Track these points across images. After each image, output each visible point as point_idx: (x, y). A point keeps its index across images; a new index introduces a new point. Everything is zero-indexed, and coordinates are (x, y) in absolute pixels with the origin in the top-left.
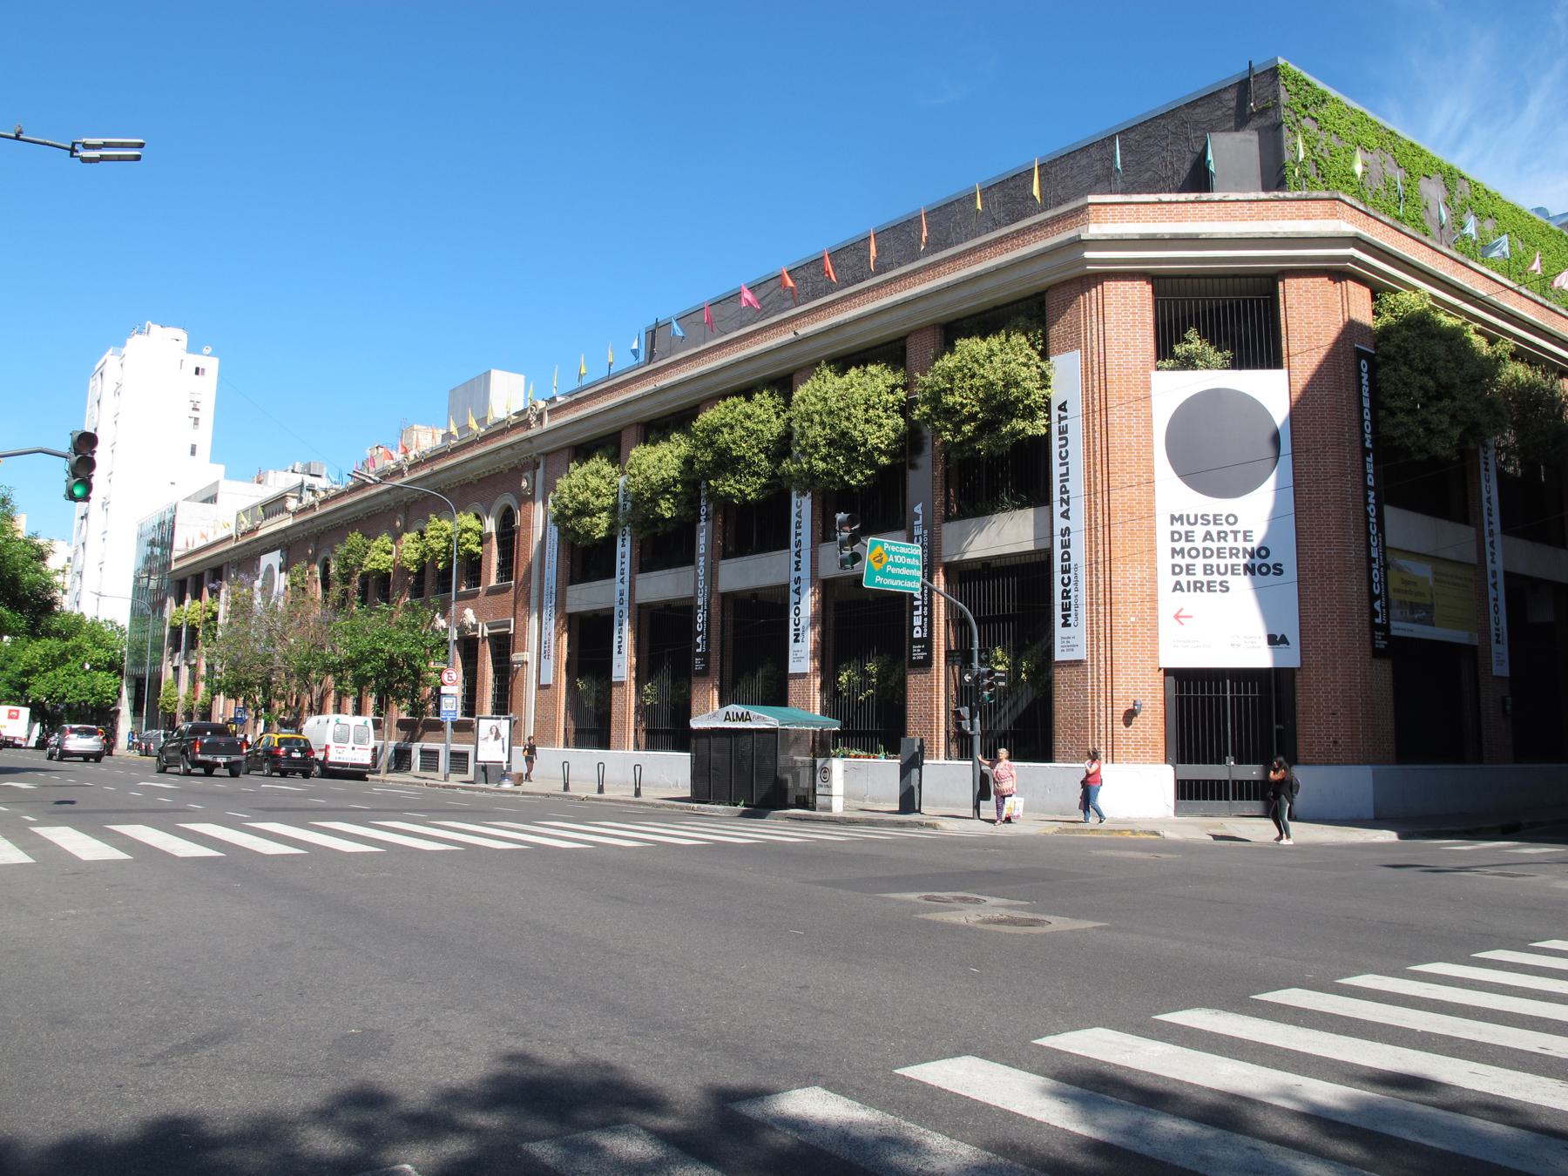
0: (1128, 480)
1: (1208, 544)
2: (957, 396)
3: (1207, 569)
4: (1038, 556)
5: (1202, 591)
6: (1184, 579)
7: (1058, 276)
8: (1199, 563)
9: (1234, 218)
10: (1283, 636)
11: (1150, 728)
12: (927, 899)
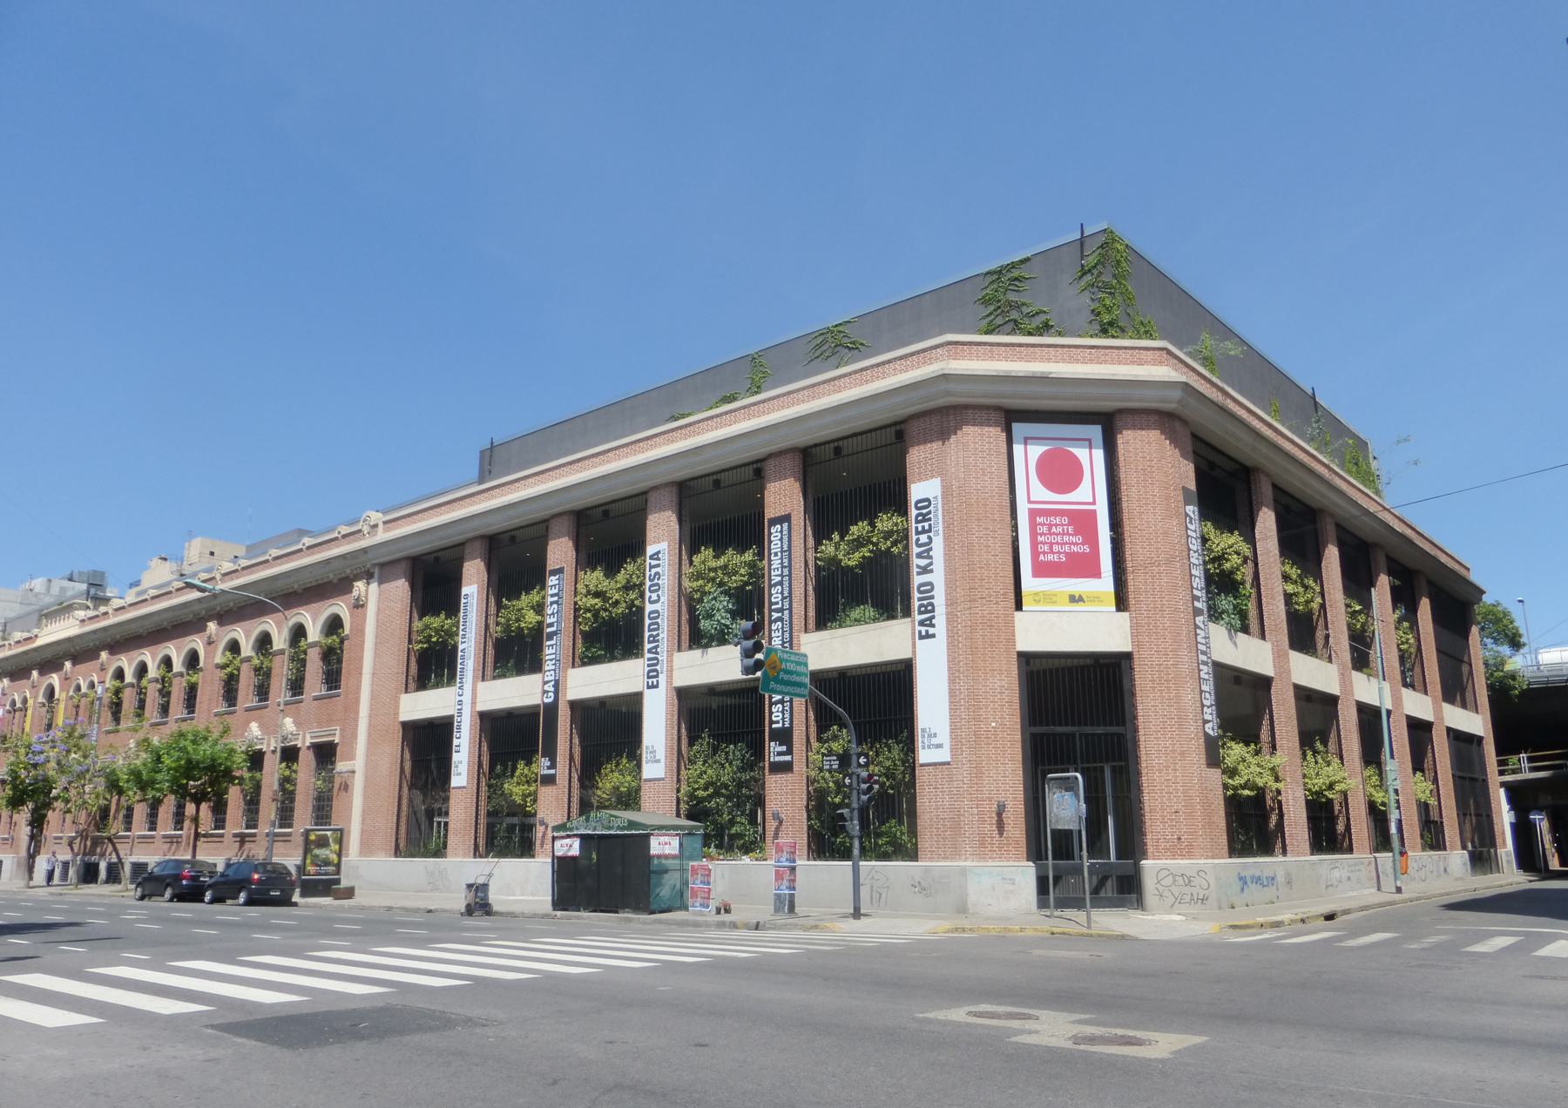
4: (874, 668)
7: (920, 406)
9: (1077, 361)
11: (1012, 827)
12: (977, 1015)
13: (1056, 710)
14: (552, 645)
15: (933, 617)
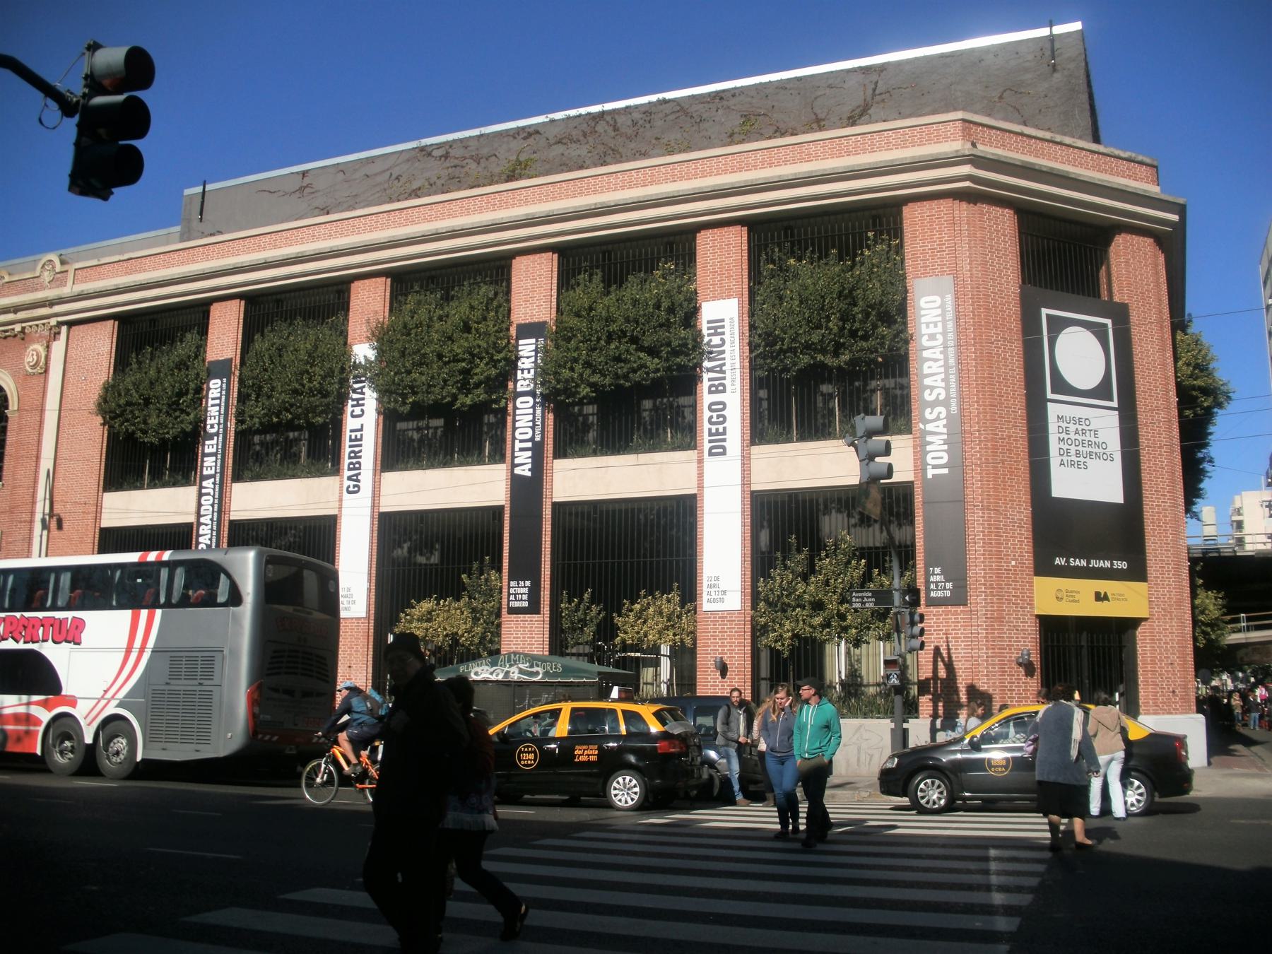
0: (1006, 414)
1: (1077, 436)
2: (307, 387)
3: (1078, 454)
5: (360, 451)
6: (1065, 458)
8: (1073, 448)
10: (1105, 593)
13: (1101, 655)
14: (213, 445)
15: (359, 474)
